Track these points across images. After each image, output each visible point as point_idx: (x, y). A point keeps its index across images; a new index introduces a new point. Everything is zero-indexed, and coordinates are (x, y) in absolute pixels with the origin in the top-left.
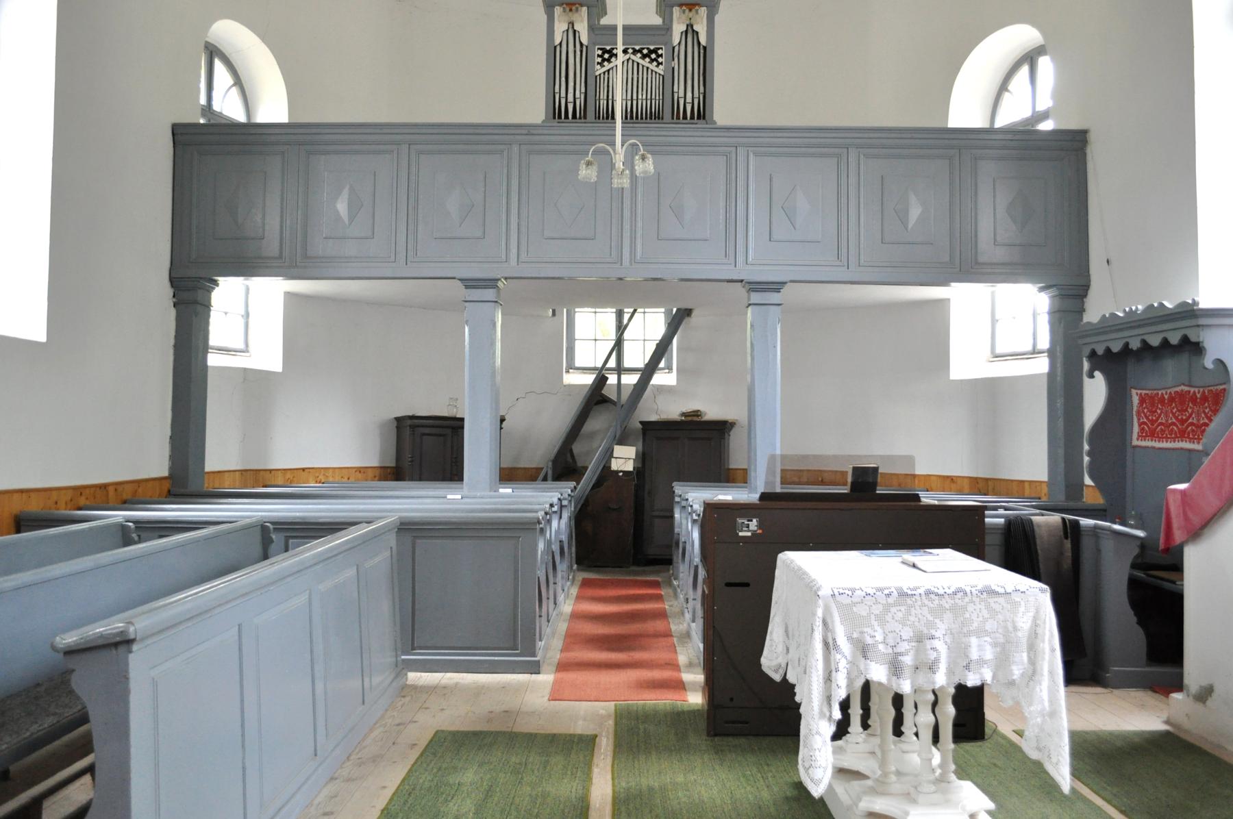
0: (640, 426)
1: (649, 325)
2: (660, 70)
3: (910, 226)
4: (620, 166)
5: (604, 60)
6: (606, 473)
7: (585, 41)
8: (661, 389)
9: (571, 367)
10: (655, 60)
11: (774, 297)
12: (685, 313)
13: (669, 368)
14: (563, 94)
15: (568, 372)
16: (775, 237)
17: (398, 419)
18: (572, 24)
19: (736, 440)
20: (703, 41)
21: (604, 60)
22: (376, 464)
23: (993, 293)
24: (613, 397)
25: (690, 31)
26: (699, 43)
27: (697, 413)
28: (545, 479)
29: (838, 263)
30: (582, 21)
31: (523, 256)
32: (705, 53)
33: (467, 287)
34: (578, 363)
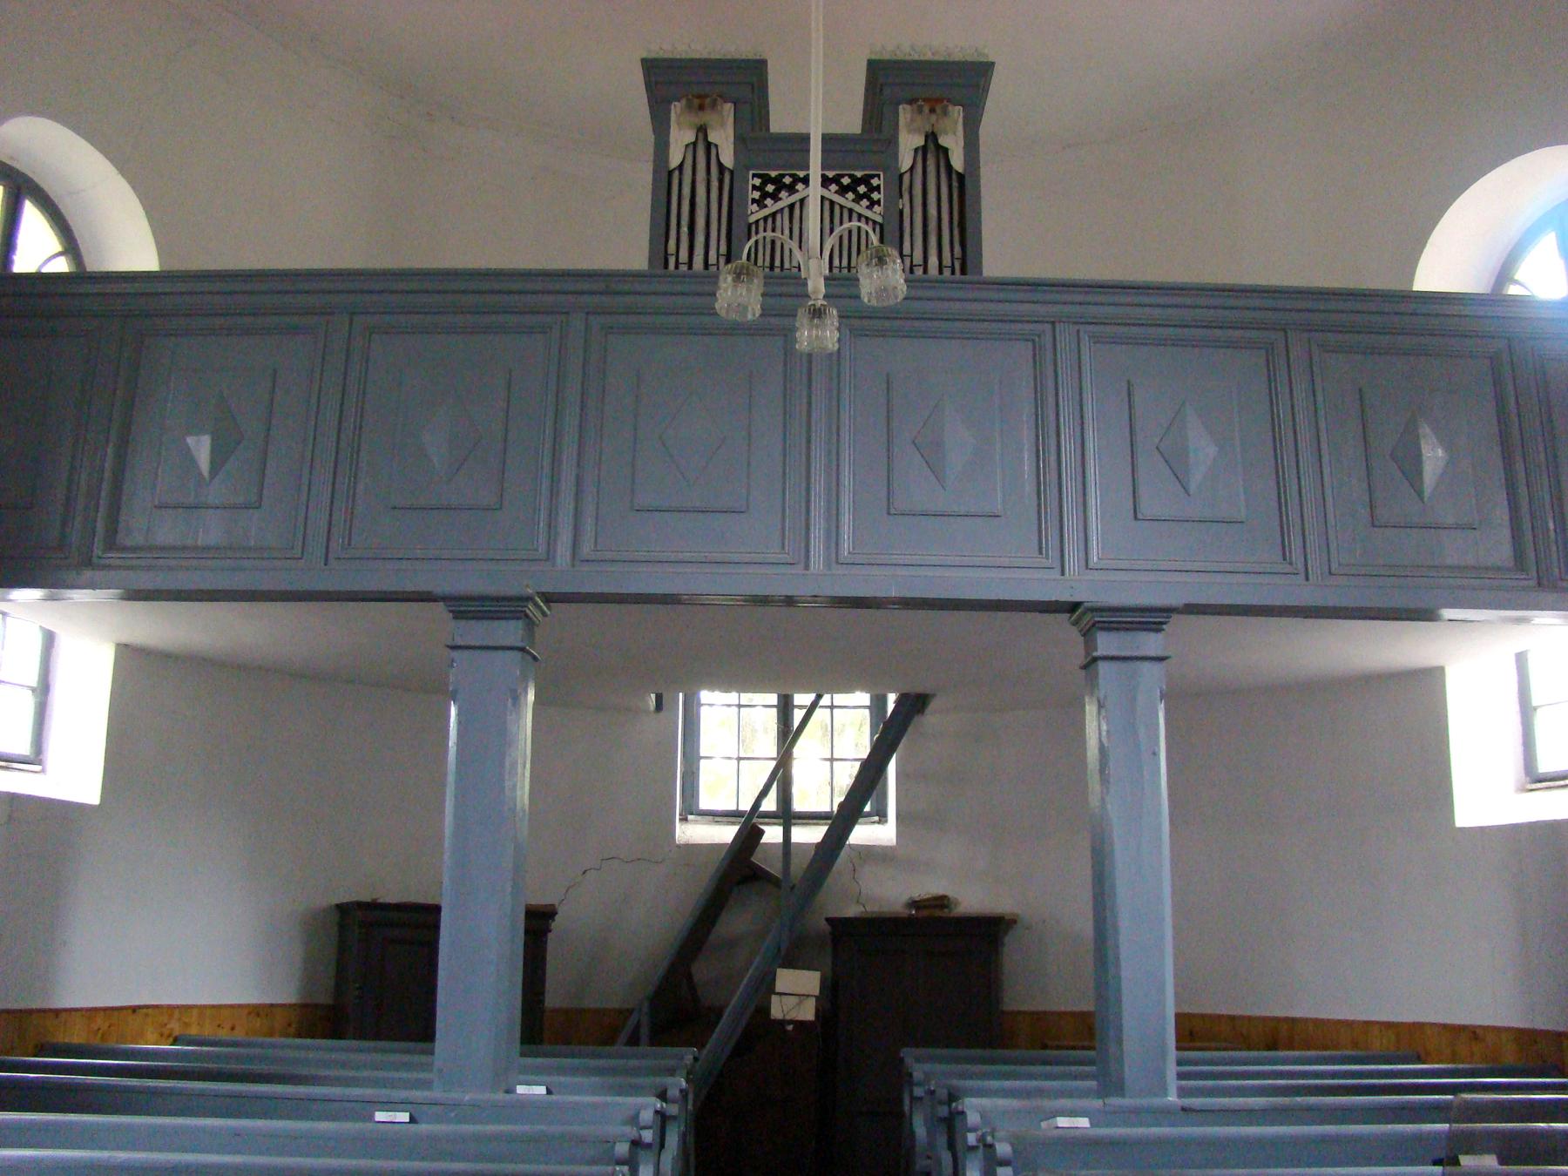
0: (828, 928)
1: (842, 729)
2: (876, 214)
3: (1427, 494)
4: (817, 285)
5: (765, 195)
6: (760, 1027)
7: (728, 159)
8: (870, 853)
9: (691, 809)
10: (866, 196)
11: (1150, 643)
12: (913, 705)
13: (882, 816)
14: (684, 256)
15: (684, 820)
16: (1146, 509)
17: (343, 910)
18: (702, 130)
19: (1012, 953)
20: (958, 163)
21: (765, 195)
22: (293, 1000)
23: (1521, 659)
24: (775, 869)
25: (932, 147)
26: (949, 167)
27: (941, 902)
28: (634, 1040)
29: (1288, 569)
30: (723, 125)
31: (586, 549)
32: (963, 188)
33: (458, 615)
34: (705, 803)
